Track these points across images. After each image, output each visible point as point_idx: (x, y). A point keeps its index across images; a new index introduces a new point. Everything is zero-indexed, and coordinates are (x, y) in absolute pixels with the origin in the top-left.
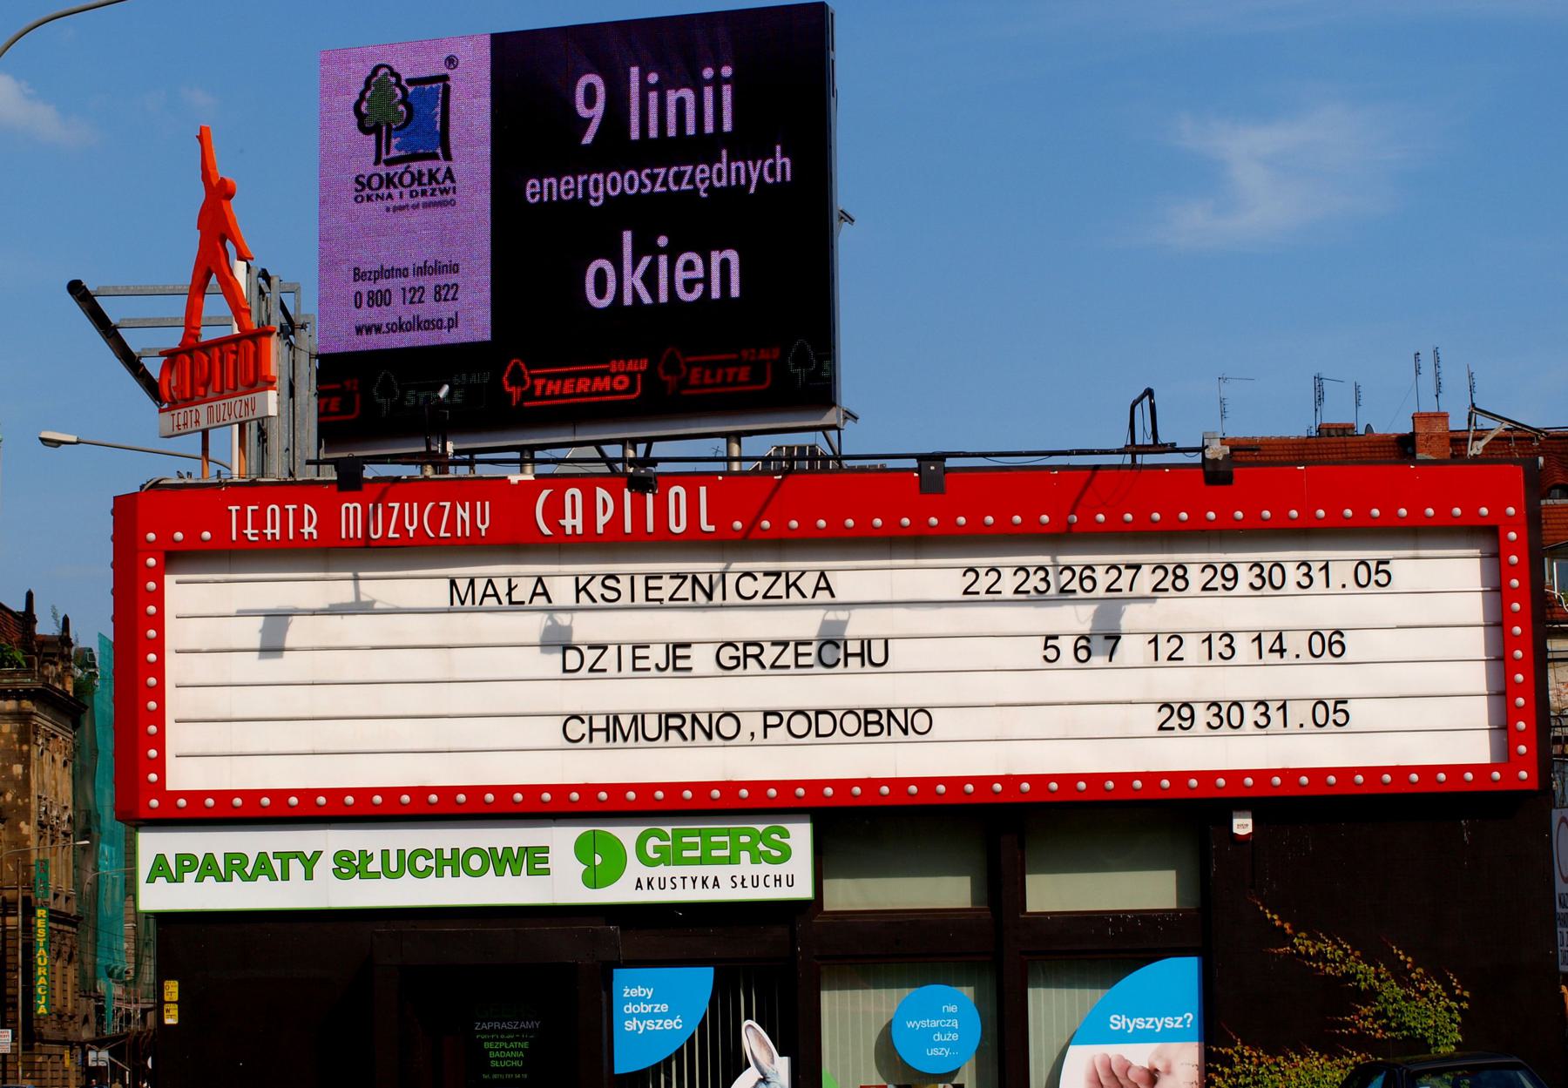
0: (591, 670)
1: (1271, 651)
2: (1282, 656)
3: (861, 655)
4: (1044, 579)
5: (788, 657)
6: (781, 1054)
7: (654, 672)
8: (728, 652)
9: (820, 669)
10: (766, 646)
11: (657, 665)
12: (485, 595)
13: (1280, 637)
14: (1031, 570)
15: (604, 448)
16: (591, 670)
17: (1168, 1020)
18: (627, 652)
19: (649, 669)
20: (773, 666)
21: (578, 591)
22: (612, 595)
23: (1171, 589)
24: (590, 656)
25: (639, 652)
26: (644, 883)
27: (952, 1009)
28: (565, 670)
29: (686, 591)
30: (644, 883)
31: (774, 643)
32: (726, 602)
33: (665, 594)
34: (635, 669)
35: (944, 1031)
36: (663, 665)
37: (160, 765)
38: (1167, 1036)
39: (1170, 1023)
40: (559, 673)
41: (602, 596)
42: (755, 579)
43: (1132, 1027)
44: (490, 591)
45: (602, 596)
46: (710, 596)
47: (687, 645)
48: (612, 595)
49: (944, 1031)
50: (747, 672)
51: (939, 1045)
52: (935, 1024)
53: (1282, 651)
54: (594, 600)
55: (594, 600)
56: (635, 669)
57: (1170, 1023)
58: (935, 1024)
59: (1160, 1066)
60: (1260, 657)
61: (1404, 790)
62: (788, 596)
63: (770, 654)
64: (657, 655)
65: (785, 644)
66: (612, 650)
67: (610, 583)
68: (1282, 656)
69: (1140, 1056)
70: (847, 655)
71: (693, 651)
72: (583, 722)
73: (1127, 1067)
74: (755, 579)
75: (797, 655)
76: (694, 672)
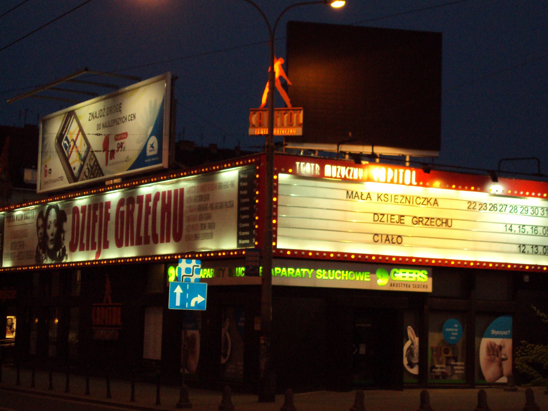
0: (380, 221)
1: (509, 229)
2: (511, 231)
3: (446, 223)
4: (486, 206)
5: (429, 223)
6: (417, 336)
7: (395, 223)
8: (415, 219)
9: (436, 226)
10: (424, 218)
11: (396, 221)
12: (355, 196)
13: (511, 226)
14: (472, 203)
15: (80, 136)
16: (380, 221)
17: (504, 332)
18: (389, 216)
19: (394, 222)
20: (425, 225)
21: (378, 198)
22: (386, 200)
23: (514, 212)
24: (381, 217)
25: (392, 217)
26: (392, 285)
27: (456, 326)
28: (374, 221)
29: (404, 201)
30: (392, 285)
31: (426, 218)
32: (413, 205)
33: (399, 201)
34: (391, 222)
35: (454, 332)
36: (398, 221)
37: (275, 240)
38: (503, 337)
39: (505, 333)
40: (372, 221)
41: (384, 200)
42: (420, 199)
43: (502, 334)
44: (357, 195)
45: (384, 200)
46: (409, 202)
47: (403, 216)
48: (386, 200)
49: (454, 332)
50: (442, 227)
51: (454, 336)
52: (452, 330)
53: (511, 230)
54: (382, 201)
55: (382, 201)
56: (391, 222)
57: (505, 333)
58: (452, 330)
59: (502, 345)
60: (506, 231)
61: (463, 267)
62: (406, 203)
63: (425, 220)
64: (396, 218)
65: (428, 218)
66: (386, 216)
67: (386, 196)
68: (511, 231)
69: (498, 341)
70: (443, 223)
71: (405, 218)
72: (440, 220)
73: (495, 345)
74: (420, 199)
75: (431, 222)
76: (405, 224)
